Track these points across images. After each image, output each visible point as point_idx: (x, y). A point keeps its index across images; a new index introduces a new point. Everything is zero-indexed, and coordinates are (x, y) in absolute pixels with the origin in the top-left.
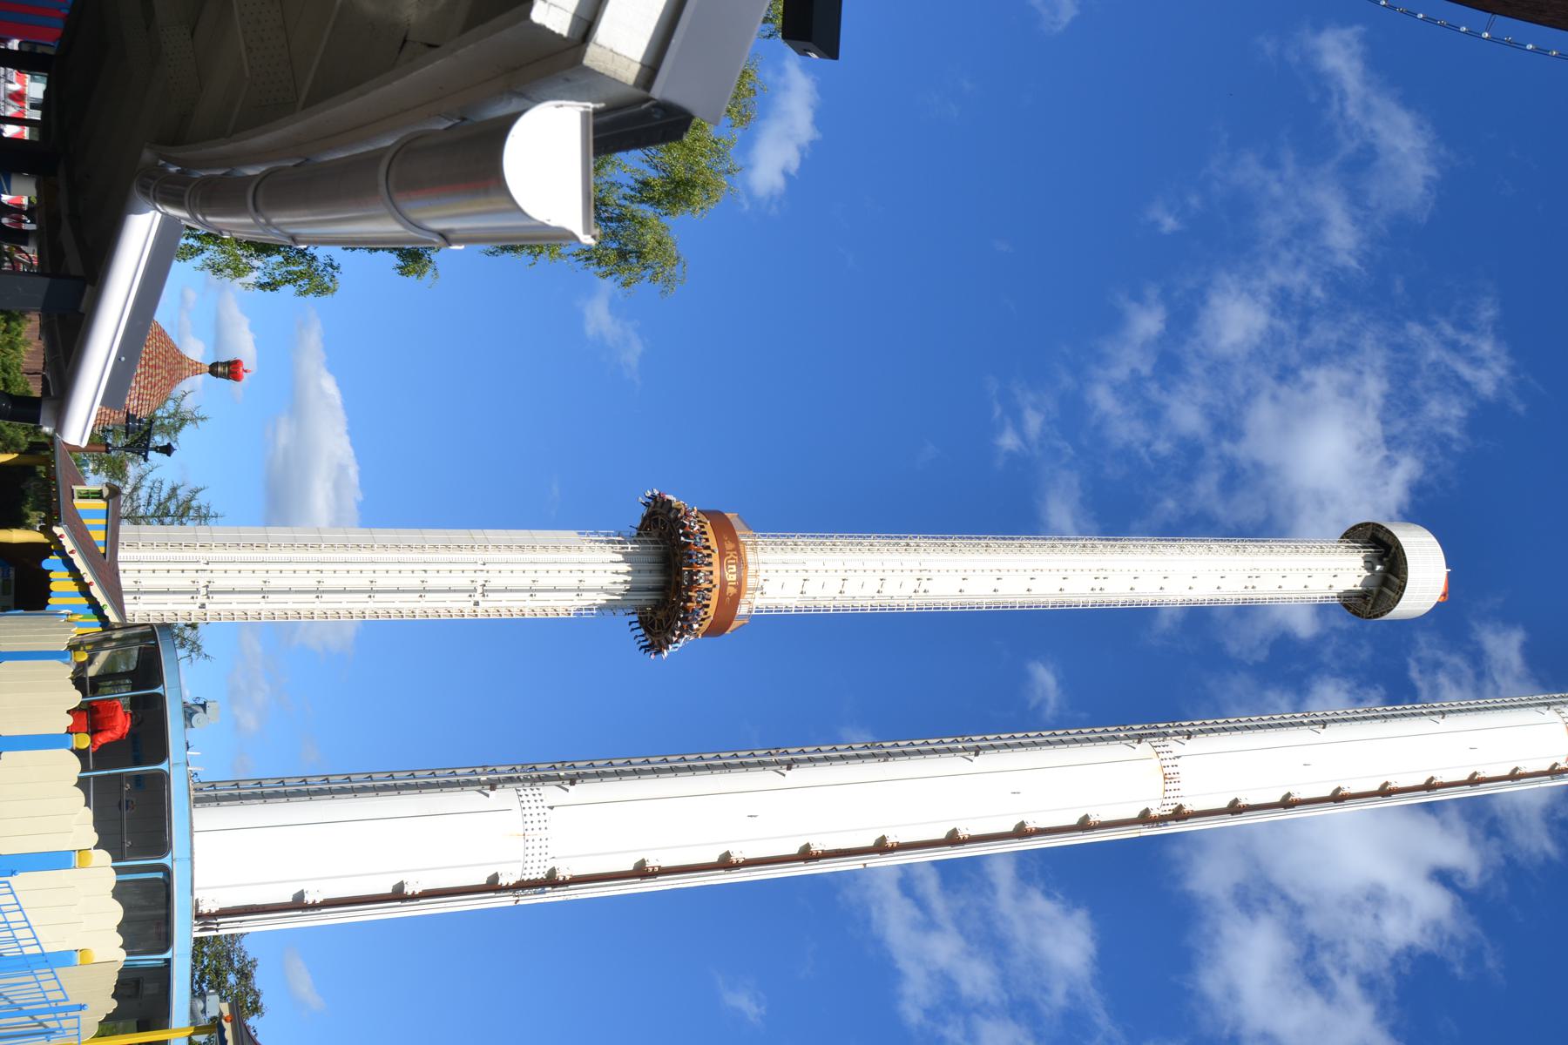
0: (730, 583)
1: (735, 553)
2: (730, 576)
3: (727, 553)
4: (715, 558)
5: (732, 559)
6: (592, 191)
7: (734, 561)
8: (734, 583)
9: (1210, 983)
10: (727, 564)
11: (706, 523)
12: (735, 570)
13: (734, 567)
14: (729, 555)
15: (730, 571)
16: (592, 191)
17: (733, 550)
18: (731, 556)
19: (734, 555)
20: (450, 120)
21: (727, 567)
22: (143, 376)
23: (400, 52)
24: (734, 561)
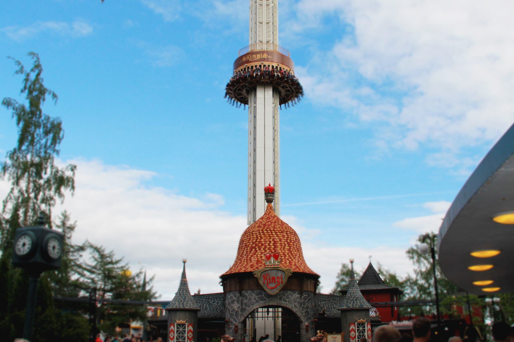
0: (261, 57)
1: (247, 56)
2: (257, 57)
3: (247, 60)
4: (249, 65)
5: (250, 57)
6: (265, 19)
7: (251, 56)
8: (261, 55)
9: (56, 241)
10: (252, 59)
11: (247, 66)
12: (255, 56)
13: (253, 56)
14: (248, 59)
15: (255, 58)
16: (265, 19)
17: (246, 57)
18: (248, 58)
19: (248, 56)
20: (280, 339)
21: (253, 59)
22: (328, 306)
23: (184, 275)
24: (251, 56)
